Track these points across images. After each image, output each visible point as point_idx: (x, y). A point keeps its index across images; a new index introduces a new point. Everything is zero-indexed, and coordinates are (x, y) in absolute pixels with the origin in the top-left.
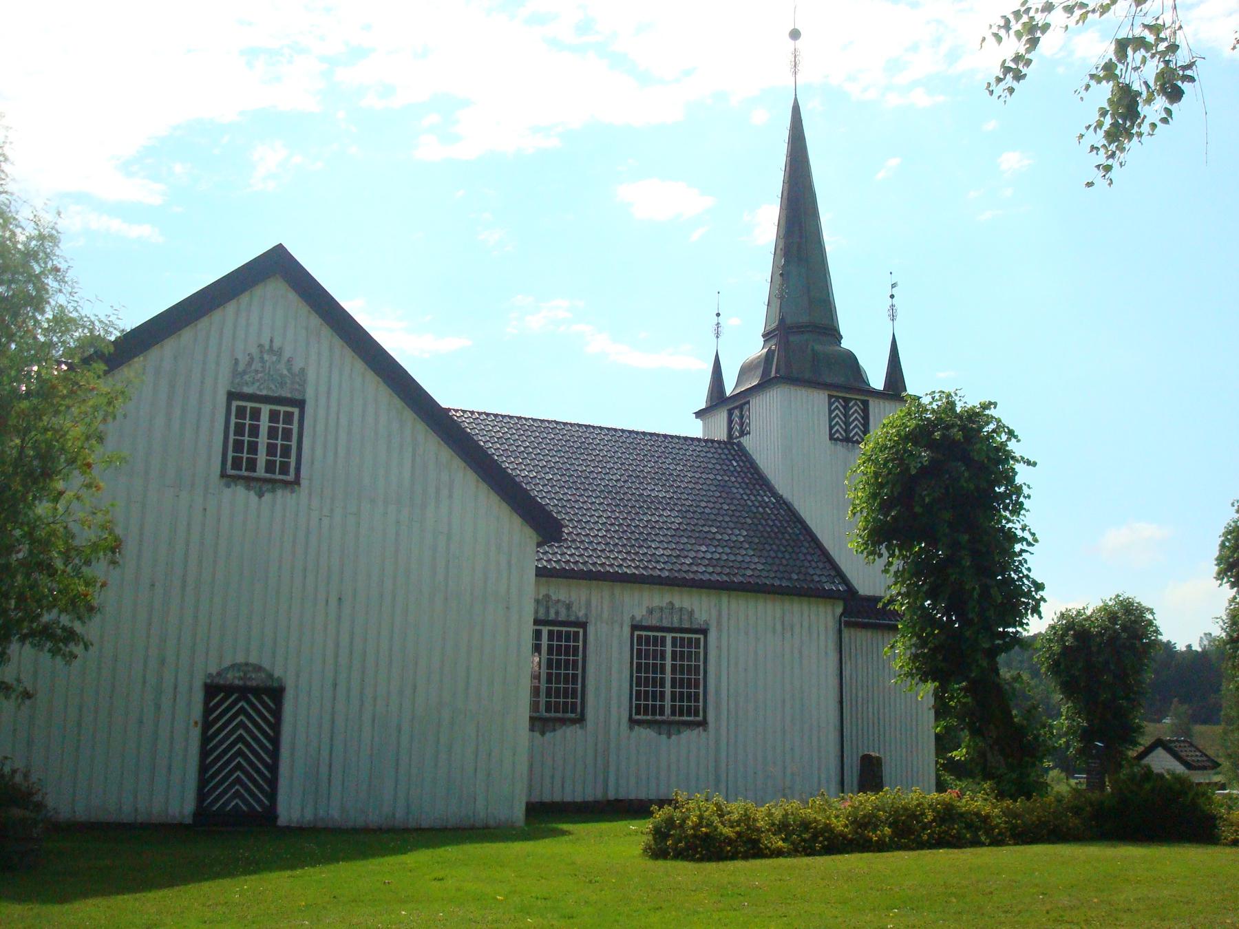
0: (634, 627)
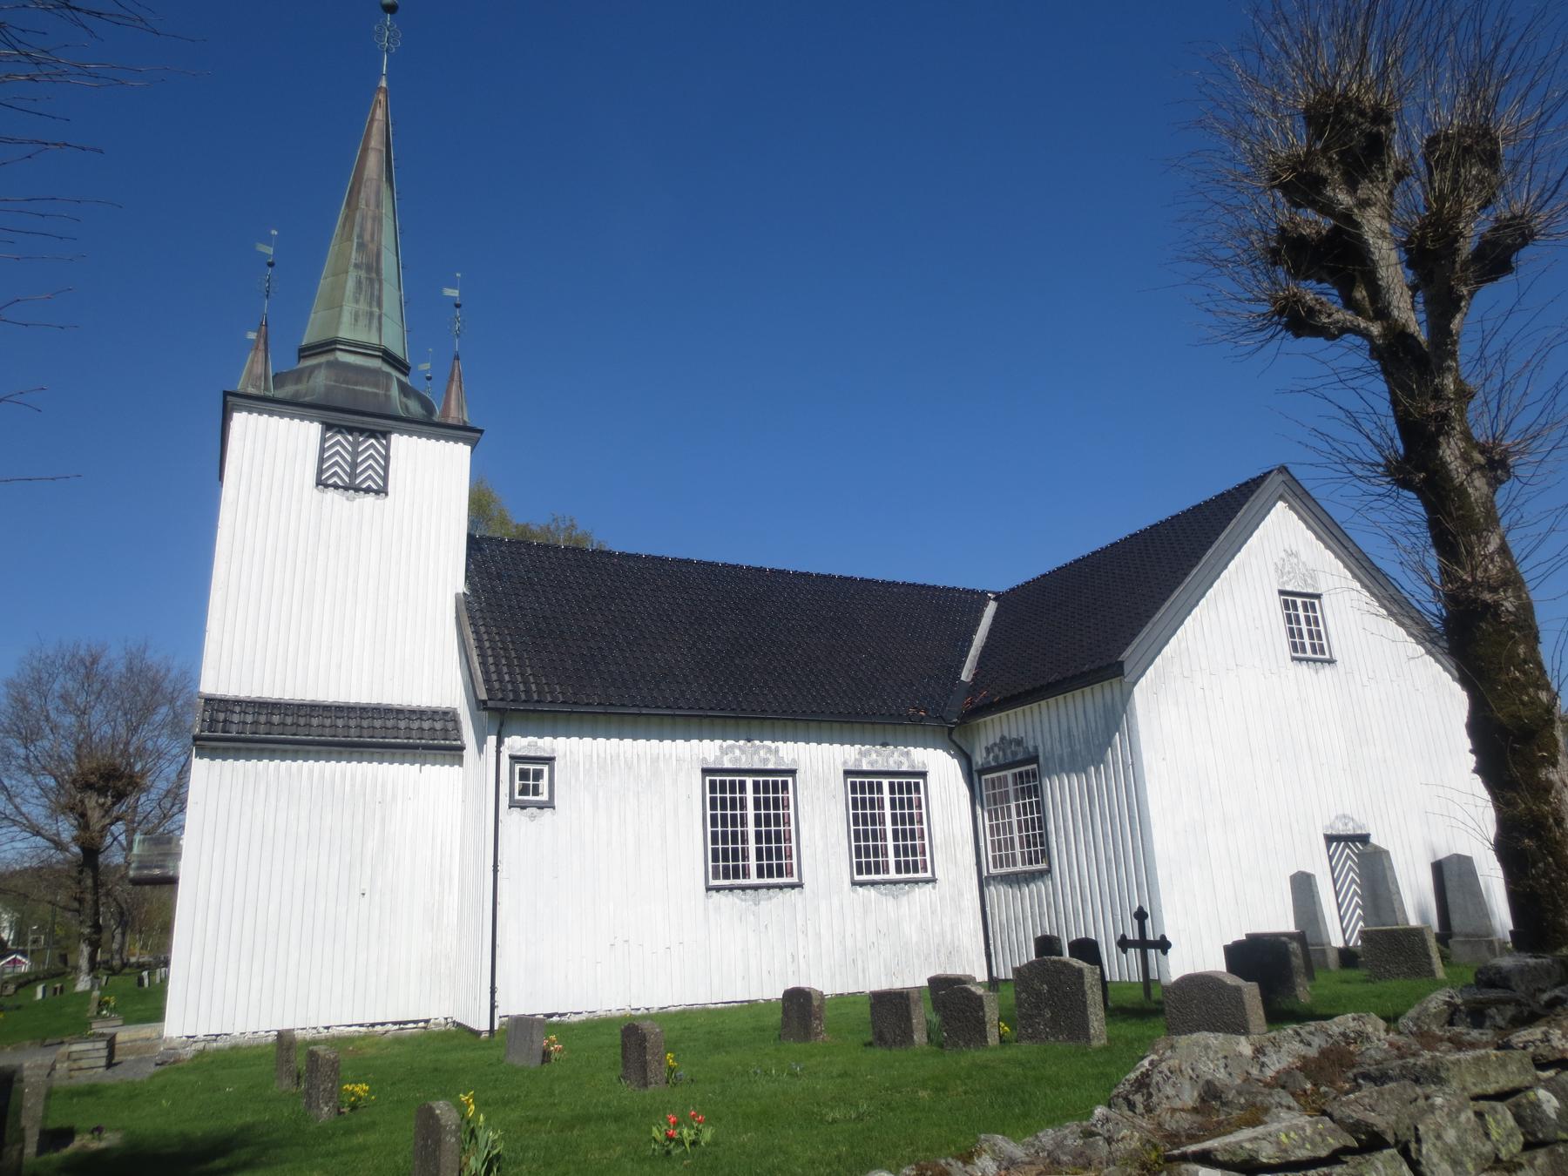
0: (847, 773)
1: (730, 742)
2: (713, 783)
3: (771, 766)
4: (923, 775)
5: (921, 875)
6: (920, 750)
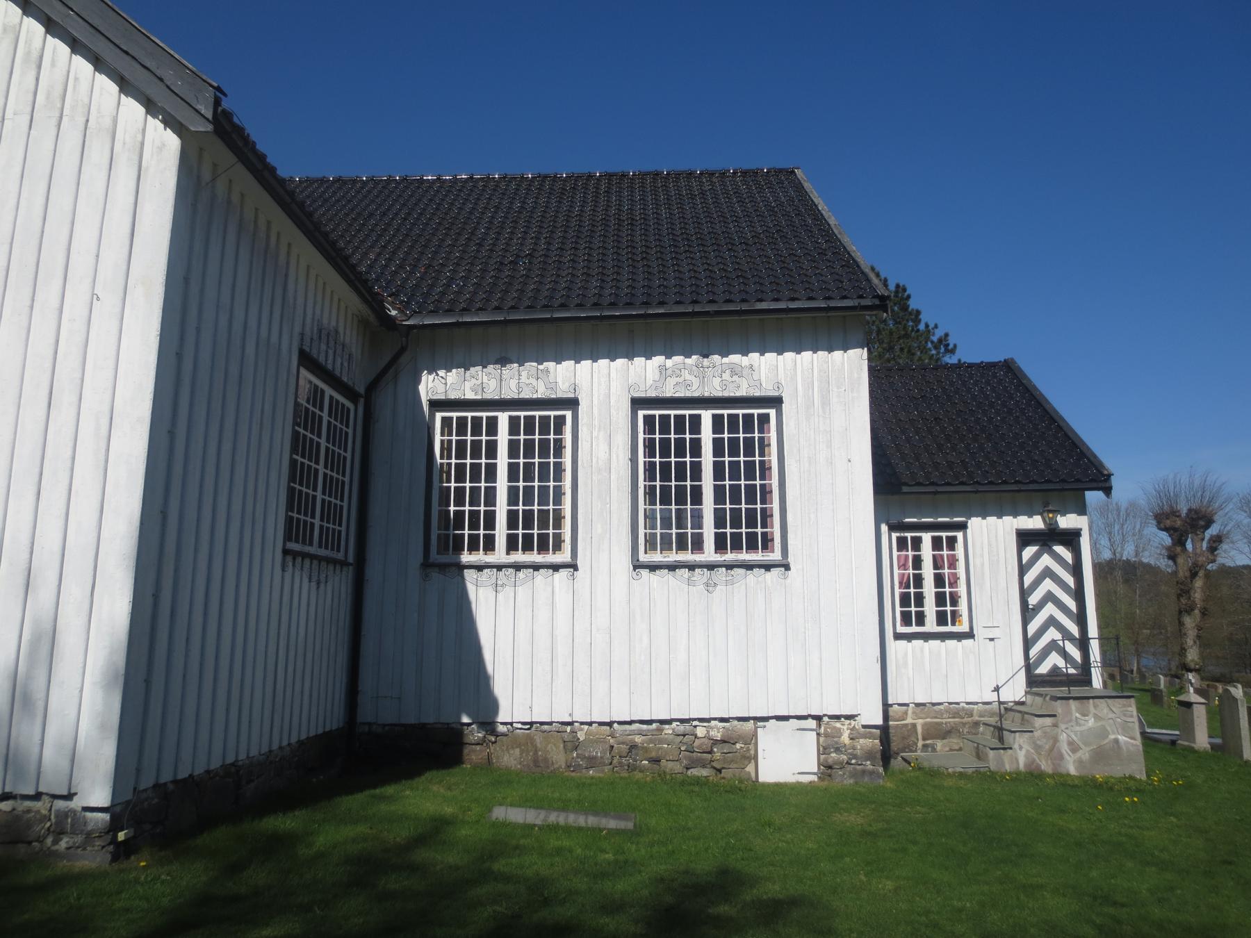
0: (637, 403)
1: (678, 359)
2: (649, 420)
3: (742, 392)
4: (776, 402)
5: (551, 558)
6: (568, 364)
